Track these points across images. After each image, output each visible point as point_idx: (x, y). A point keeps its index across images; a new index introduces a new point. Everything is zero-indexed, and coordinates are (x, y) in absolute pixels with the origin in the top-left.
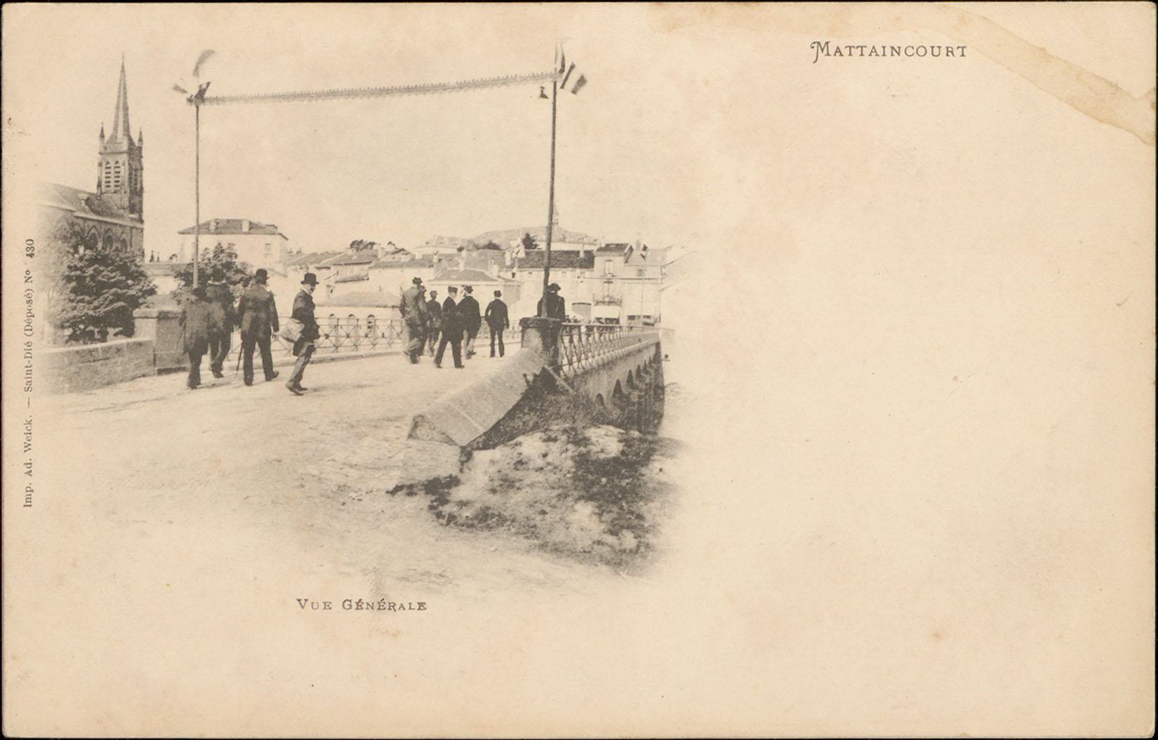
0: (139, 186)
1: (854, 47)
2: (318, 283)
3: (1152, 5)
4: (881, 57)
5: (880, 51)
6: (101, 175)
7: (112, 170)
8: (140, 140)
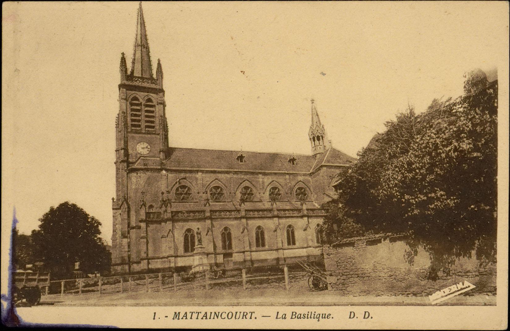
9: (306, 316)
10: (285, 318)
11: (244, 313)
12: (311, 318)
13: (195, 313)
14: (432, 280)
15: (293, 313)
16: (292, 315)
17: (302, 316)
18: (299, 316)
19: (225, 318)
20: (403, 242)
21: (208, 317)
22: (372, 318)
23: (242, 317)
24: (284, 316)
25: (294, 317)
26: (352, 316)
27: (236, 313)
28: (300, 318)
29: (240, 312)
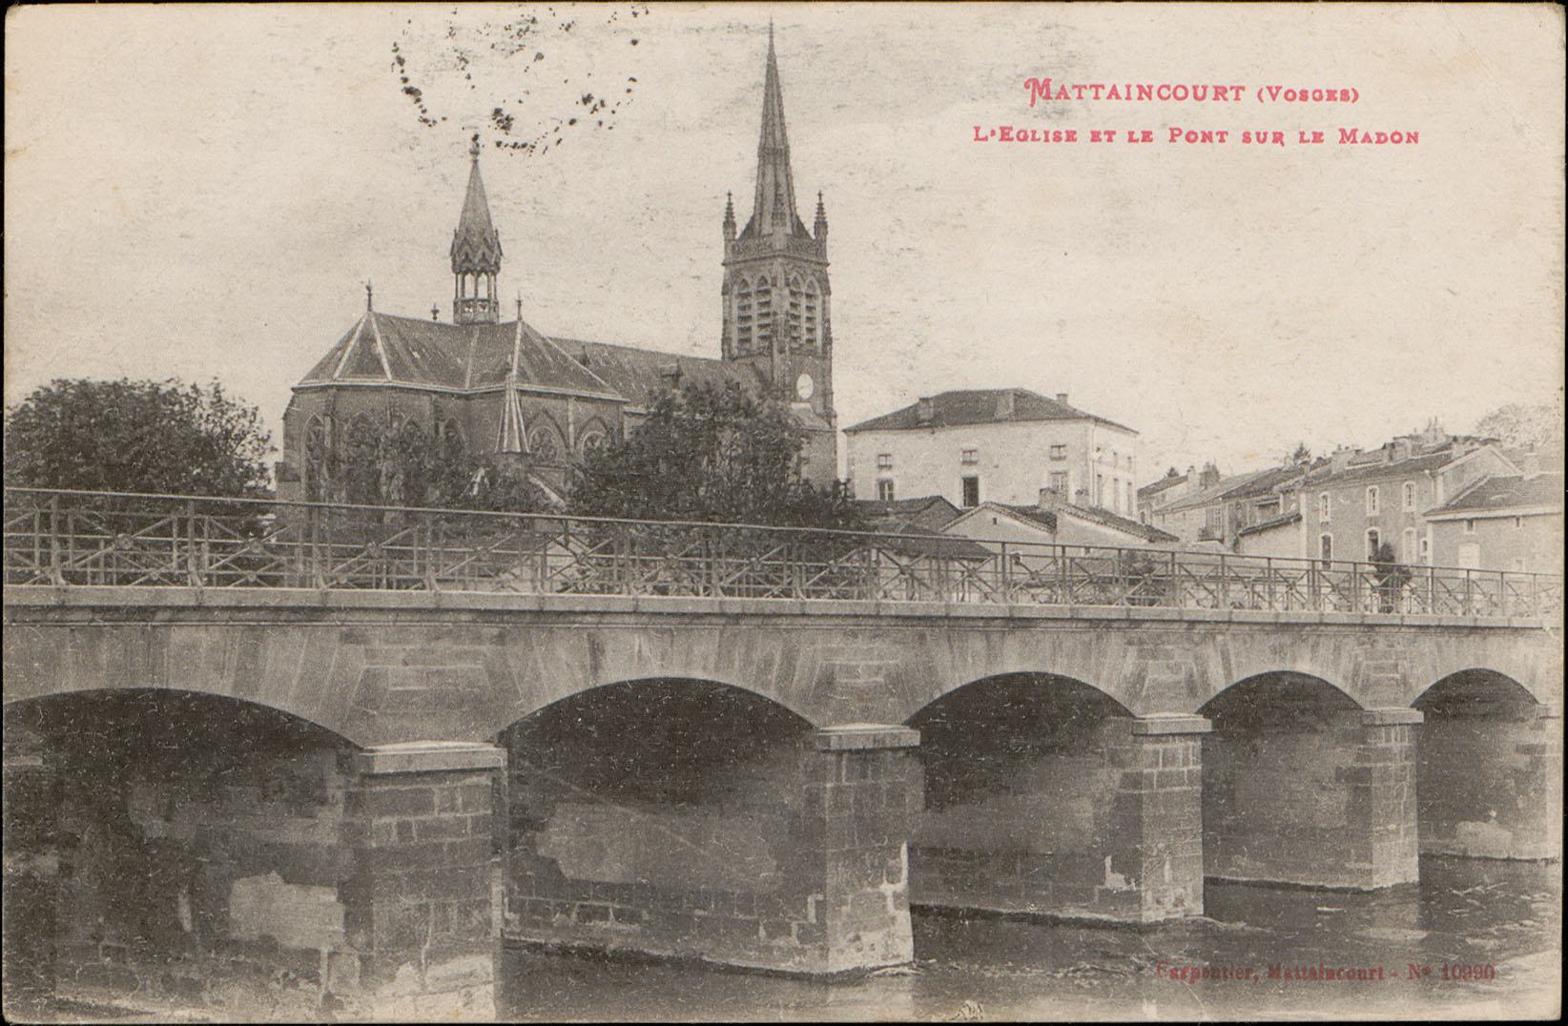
0: (819, 333)
1: (1085, 87)
2: (293, 389)
3: (1561, 8)
4: (1124, 101)
5: (1122, 92)
6: (730, 314)
7: (754, 301)
8: (821, 224)
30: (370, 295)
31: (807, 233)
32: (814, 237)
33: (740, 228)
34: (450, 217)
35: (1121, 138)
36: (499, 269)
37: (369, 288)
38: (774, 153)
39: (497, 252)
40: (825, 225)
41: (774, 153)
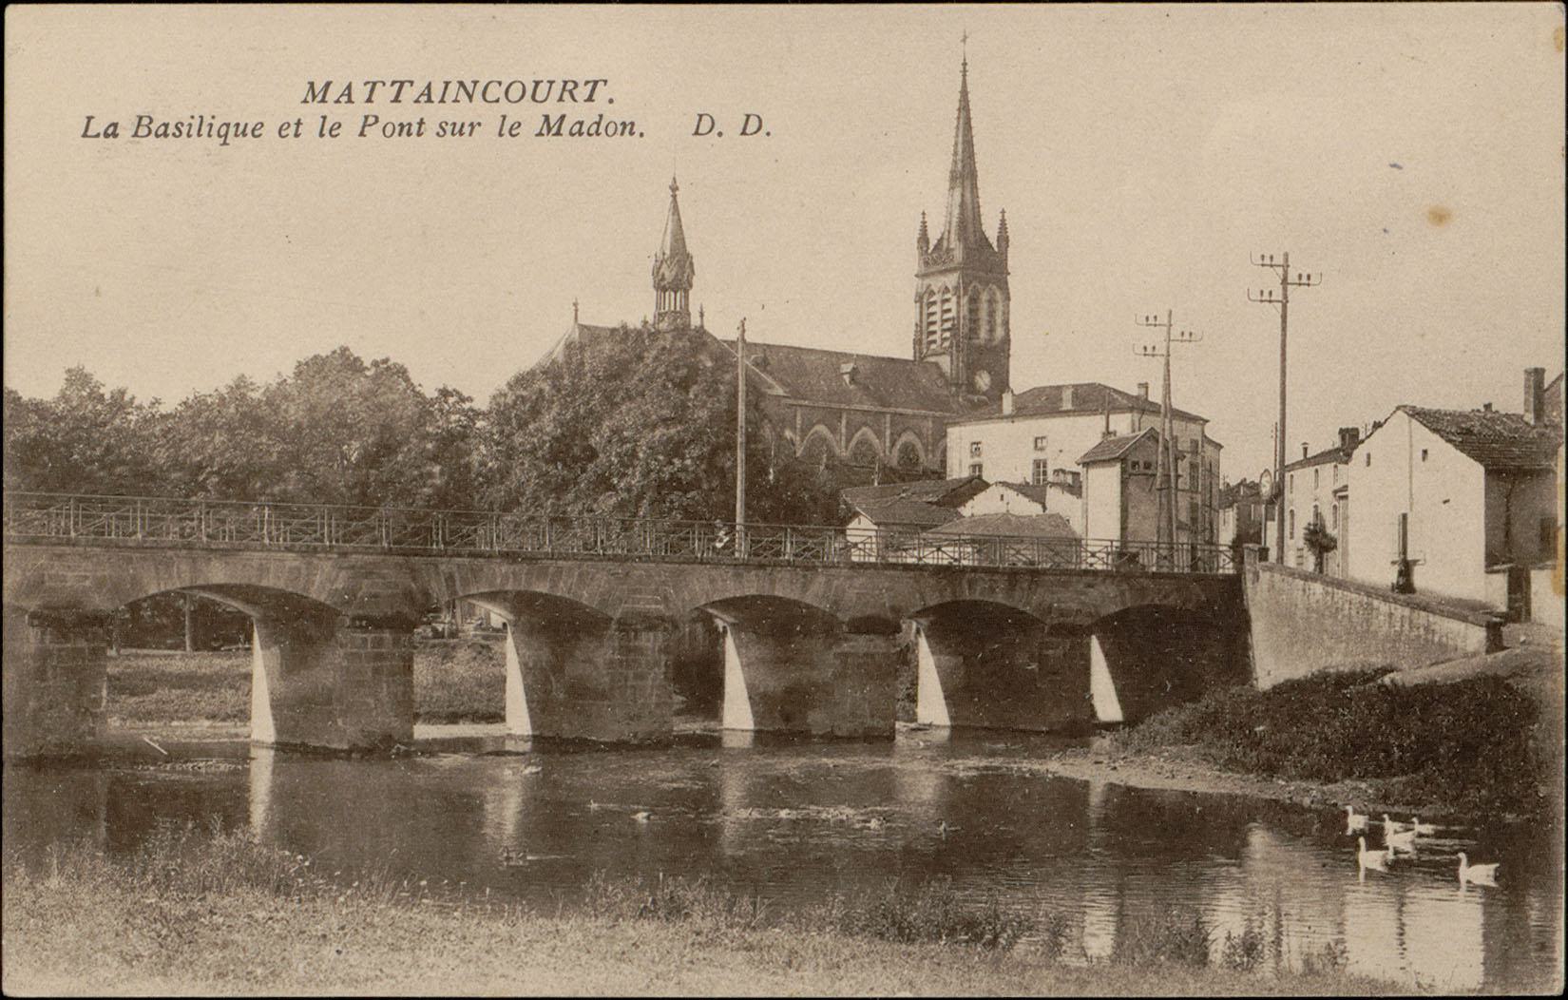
8: (1004, 238)
9: (185, 130)
10: (115, 135)
11: (565, 83)
12: (199, 135)
13: (388, 84)
14: (573, 606)
15: (141, 118)
16: (139, 125)
17: (171, 130)
18: (161, 131)
19: (497, 101)
20: (1564, 369)
21: (436, 96)
22: (720, 134)
23: (557, 97)
24: (110, 131)
25: (143, 131)
26: (705, 127)
27: (537, 83)
28: (165, 134)
29: (551, 83)
30: (576, 310)
31: (991, 246)
32: (996, 249)
33: (933, 242)
34: (658, 242)
35: (270, 131)
36: (691, 286)
37: (575, 305)
38: (965, 174)
39: (688, 271)
40: (1007, 240)
41: (965, 174)
